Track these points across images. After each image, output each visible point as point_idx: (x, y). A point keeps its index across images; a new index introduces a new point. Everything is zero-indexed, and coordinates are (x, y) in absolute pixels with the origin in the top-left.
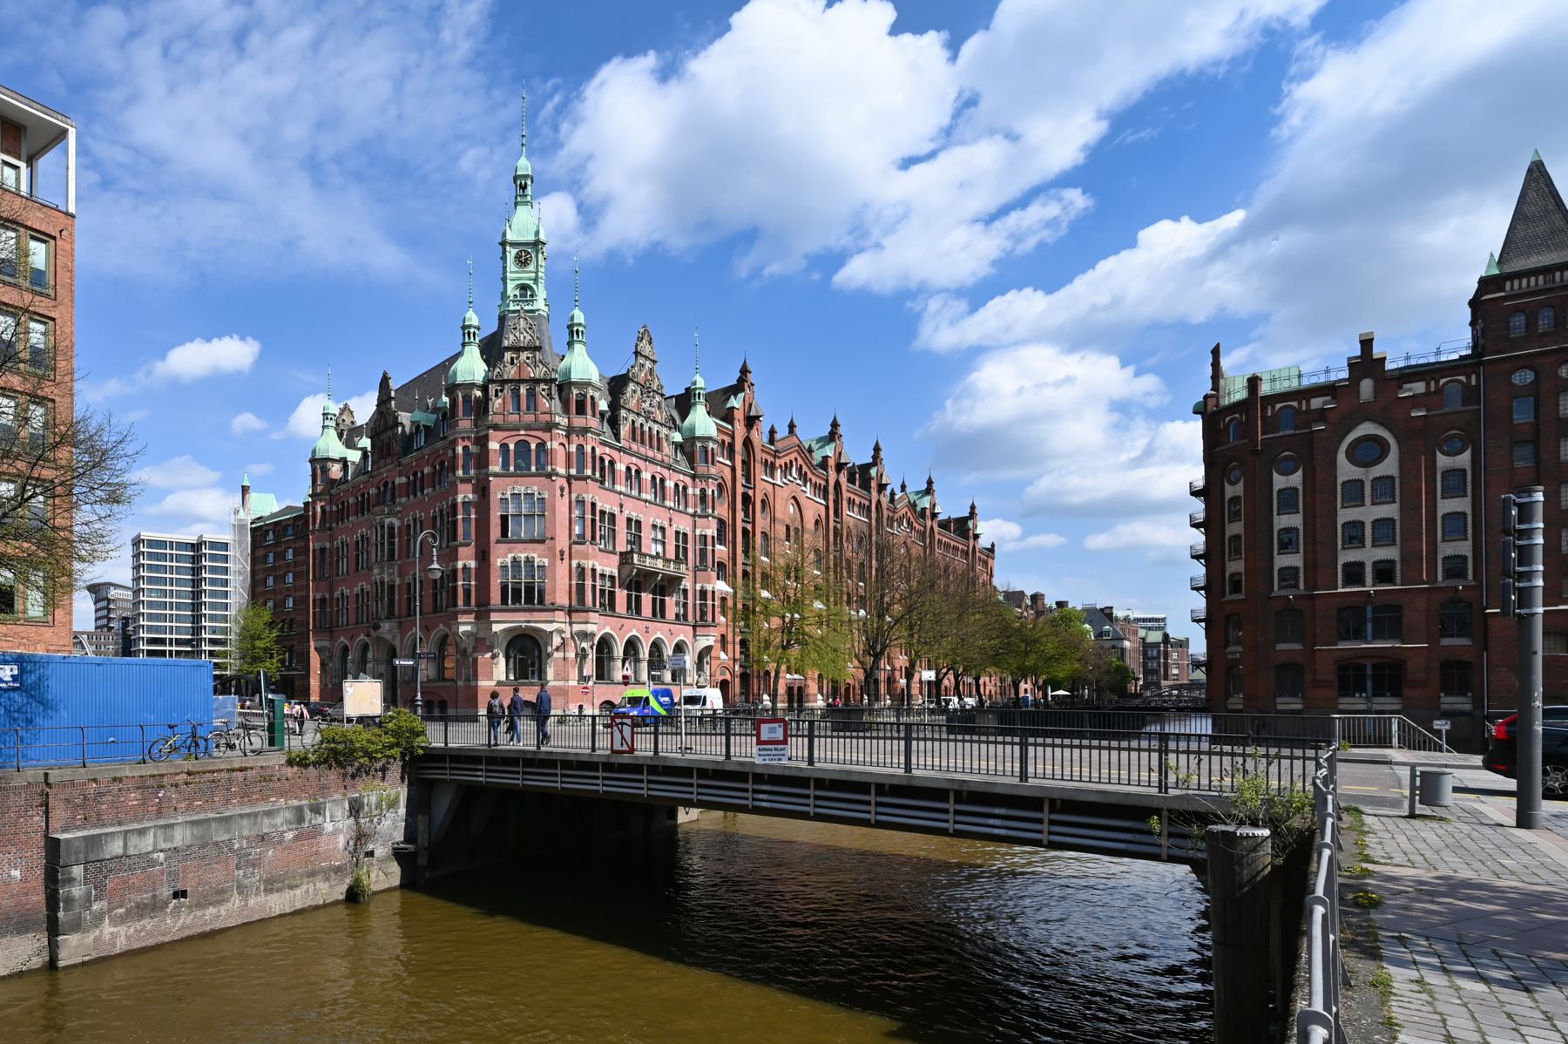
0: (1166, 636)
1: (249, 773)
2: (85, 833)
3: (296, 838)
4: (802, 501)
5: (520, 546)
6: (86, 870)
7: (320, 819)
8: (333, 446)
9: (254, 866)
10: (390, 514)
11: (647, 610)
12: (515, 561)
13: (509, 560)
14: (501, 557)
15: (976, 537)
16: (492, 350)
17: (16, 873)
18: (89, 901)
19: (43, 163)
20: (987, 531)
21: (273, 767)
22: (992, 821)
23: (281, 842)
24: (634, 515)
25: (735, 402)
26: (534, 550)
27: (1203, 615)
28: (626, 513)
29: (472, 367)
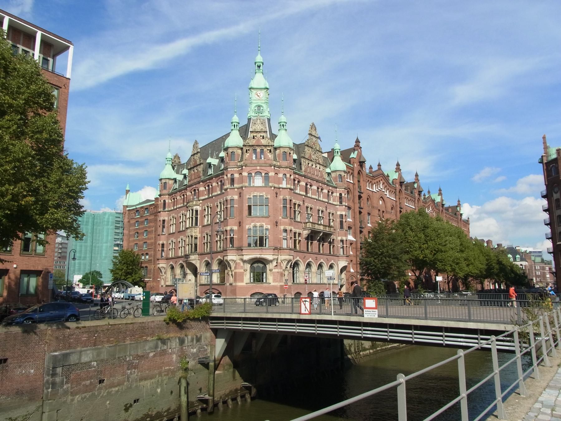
0: (542, 260)
1: (135, 326)
2: (64, 352)
3: (154, 356)
4: (385, 199)
5: (257, 219)
6: (62, 369)
7: (165, 347)
8: (168, 172)
9: (135, 368)
10: (196, 205)
11: (117, 231)
12: (255, 226)
13: (252, 226)
14: (249, 225)
15: (461, 215)
16: (244, 131)
17: (32, 371)
18: (63, 384)
19: (58, 58)
20: (466, 211)
21: (145, 323)
22: (459, 340)
23: (147, 358)
24: (310, 205)
25: (353, 155)
26: (263, 222)
27: (551, 250)
28: (306, 204)
29: (235, 140)
